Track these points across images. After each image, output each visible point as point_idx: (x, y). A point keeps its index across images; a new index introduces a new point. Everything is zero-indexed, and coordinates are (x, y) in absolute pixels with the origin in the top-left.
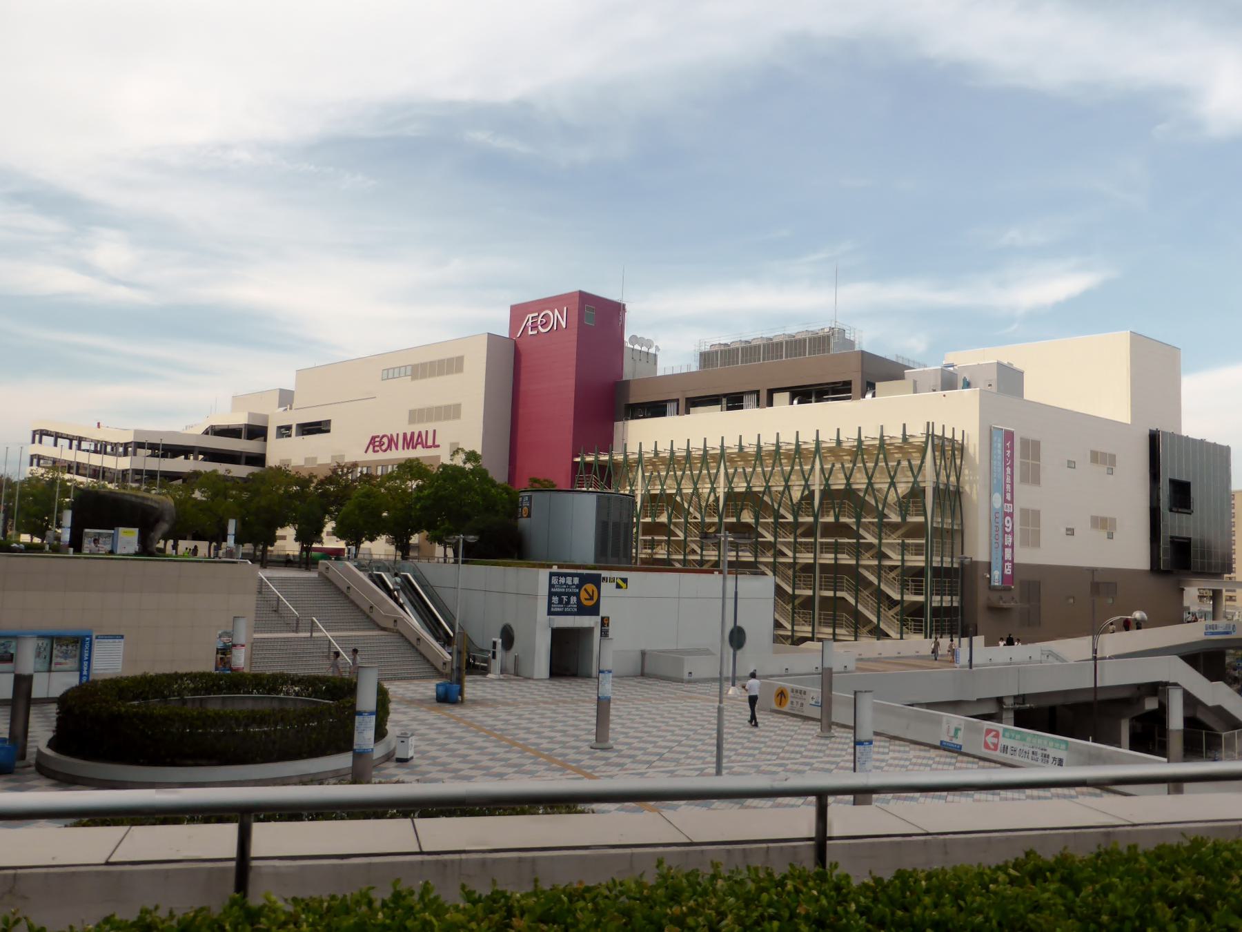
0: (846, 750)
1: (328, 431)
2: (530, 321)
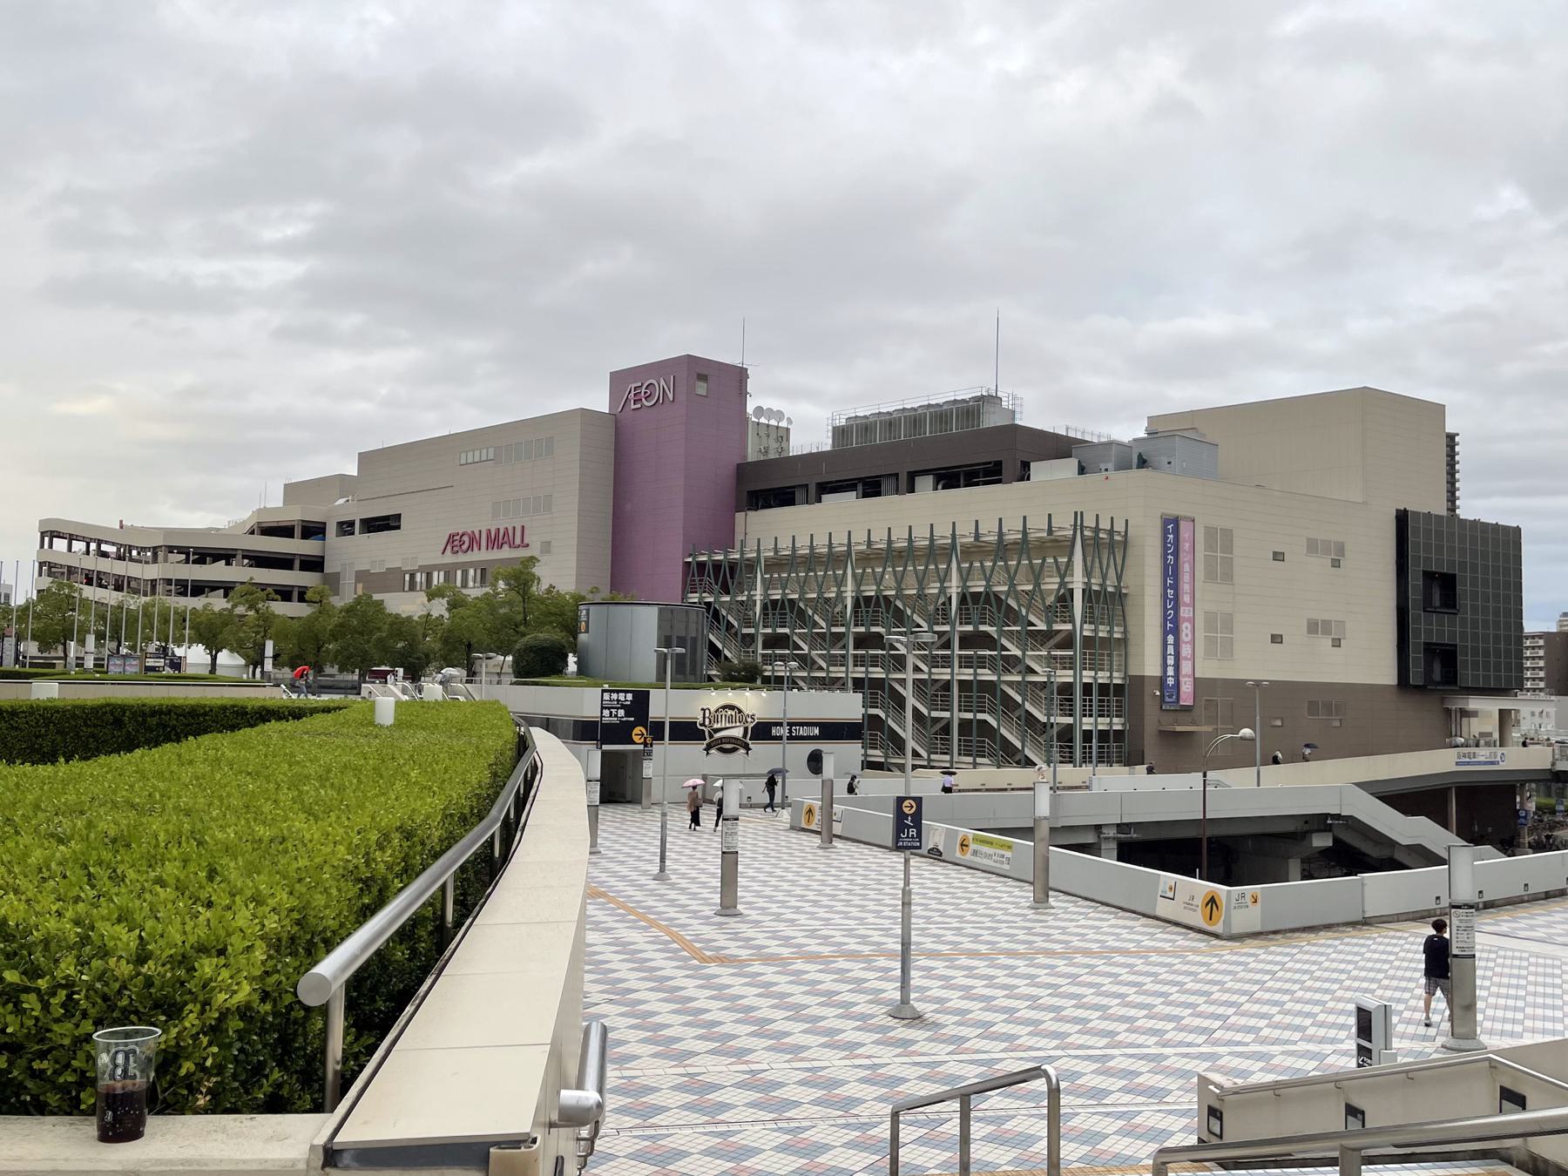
0: (1411, 990)
1: (398, 527)
2: (633, 393)
